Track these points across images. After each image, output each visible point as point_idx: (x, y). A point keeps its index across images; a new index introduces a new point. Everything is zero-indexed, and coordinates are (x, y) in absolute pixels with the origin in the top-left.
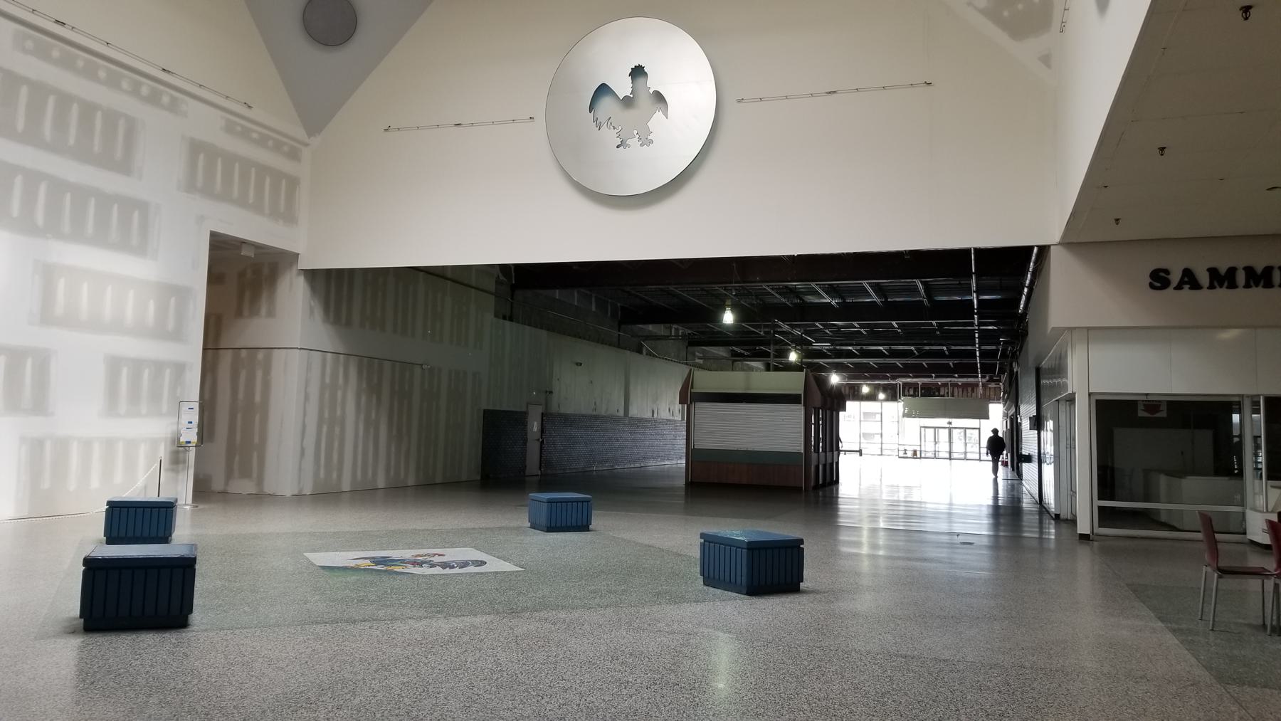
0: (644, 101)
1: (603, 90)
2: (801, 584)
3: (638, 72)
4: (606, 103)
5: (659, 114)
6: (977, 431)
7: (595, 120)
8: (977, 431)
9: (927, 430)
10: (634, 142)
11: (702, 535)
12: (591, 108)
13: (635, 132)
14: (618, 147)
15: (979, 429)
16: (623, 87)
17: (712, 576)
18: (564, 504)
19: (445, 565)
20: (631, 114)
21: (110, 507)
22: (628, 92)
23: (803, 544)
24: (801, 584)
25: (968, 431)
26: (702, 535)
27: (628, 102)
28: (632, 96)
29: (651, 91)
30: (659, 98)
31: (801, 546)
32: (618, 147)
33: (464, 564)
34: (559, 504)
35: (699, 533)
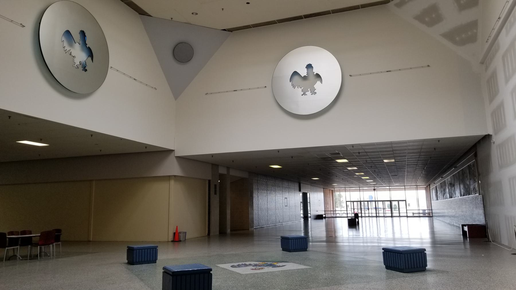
0: (312, 78)
1: (295, 73)
2: (426, 267)
3: (309, 66)
4: (296, 78)
5: (318, 83)
6: (405, 202)
7: (293, 85)
8: (405, 202)
9: (379, 202)
10: (309, 93)
11: (128, 247)
12: (291, 80)
13: (309, 89)
14: (302, 95)
15: (405, 201)
16: (303, 72)
17: (411, 267)
18: (301, 240)
19: (246, 265)
20: (306, 83)
21: (128, 249)
22: (305, 74)
23: (426, 251)
24: (426, 267)
25: (400, 202)
26: (128, 247)
27: (305, 78)
28: (307, 75)
29: (315, 74)
30: (318, 76)
31: (425, 252)
32: (302, 95)
33: (239, 266)
34: (297, 240)
35: (127, 246)
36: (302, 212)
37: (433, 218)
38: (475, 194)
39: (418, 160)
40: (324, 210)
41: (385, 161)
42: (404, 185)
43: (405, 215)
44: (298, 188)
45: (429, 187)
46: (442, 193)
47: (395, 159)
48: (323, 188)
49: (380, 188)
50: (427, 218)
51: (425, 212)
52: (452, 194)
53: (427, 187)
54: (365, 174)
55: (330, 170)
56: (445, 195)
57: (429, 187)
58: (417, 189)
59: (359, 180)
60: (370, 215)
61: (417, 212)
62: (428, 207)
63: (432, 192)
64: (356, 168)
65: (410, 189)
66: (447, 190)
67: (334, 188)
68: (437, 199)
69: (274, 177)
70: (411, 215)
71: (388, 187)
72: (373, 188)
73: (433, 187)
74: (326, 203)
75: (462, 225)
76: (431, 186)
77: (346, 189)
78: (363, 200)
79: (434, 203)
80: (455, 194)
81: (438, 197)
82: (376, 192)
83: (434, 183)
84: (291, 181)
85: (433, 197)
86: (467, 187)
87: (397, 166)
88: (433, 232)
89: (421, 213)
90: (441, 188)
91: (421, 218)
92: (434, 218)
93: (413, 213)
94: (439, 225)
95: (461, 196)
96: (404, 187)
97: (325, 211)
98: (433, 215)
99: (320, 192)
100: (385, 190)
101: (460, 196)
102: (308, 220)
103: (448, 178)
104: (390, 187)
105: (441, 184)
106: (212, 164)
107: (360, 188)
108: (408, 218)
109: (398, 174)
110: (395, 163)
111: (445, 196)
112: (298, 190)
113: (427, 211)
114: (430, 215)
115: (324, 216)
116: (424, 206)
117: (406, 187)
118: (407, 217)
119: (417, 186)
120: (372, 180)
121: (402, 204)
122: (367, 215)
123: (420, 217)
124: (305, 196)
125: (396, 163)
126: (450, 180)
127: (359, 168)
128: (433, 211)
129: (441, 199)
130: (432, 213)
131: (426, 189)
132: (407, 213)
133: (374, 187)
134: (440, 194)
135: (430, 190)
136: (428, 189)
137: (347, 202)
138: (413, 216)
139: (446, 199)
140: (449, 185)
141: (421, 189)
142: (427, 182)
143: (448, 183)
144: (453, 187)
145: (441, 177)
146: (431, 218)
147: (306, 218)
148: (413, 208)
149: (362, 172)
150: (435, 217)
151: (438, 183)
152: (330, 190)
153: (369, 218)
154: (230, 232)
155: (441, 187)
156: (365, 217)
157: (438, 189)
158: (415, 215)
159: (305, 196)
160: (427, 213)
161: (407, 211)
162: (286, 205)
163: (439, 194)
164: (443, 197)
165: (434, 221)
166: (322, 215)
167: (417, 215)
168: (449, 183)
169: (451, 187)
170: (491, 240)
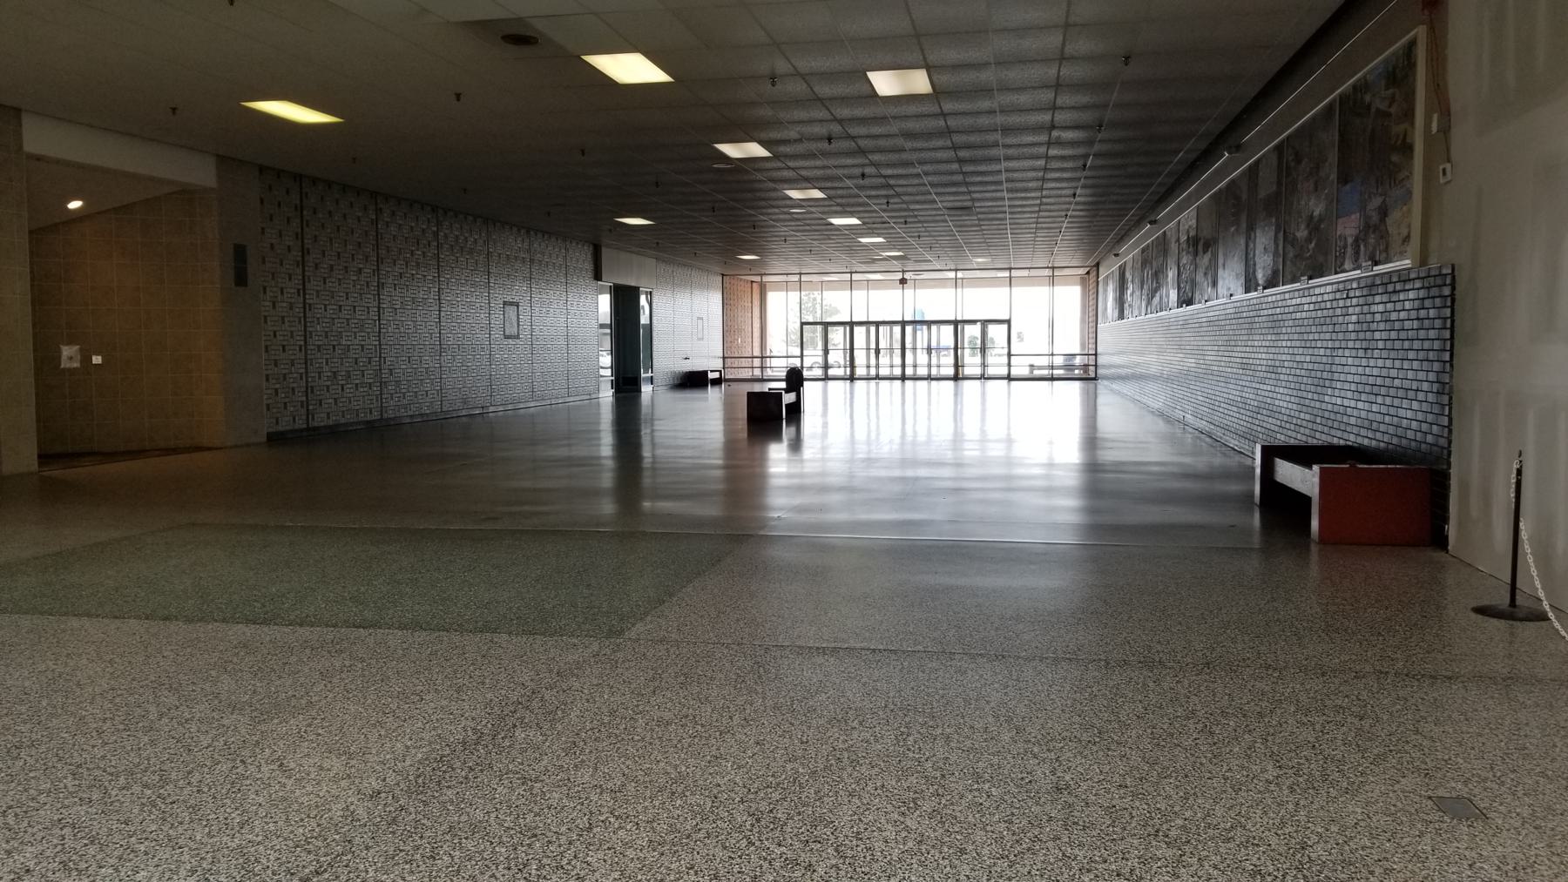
15: (1008, 322)
36: (606, 360)
37: (1099, 386)
38: (1376, 263)
39: (1058, 86)
40: (722, 355)
41: (885, 83)
42: (1006, 267)
43: (1004, 371)
44: (589, 266)
45: (1093, 274)
46: (1145, 287)
47: (930, 69)
48: (723, 275)
49: (926, 275)
50: (1077, 384)
51: (1071, 363)
52: (1194, 284)
53: (1088, 273)
54: (830, 198)
55: (774, 226)
56: (1158, 295)
57: (1095, 273)
58: (1052, 281)
59: (870, 258)
60: (934, 372)
61: (1044, 361)
62: (1083, 345)
63: (1105, 291)
64: (817, 194)
65: (1030, 281)
66: (1171, 274)
67: (761, 275)
68: (1121, 316)
69: (434, 209)
70: (1025, 372)
71: (952, 275)
72: (899, 276)
73: (1109, 269)
74: (729, 330)
75: (1264, 448)
76: (1101, 269)
77: (804, 278)
78: (865, 320)
79: (1109, 330)
80: (1215, 284)
81: (1126, 305)
82: (909, 292)
83: (1116, 255)
84: (544, 233)
85: (1106, 309)
86: (1302, 233)
87: (958, 139)
88: (1091, 440)
89: (1059, 368)
90: (1143, 271)
91: (1055, 383)
92: (1102, 384)
93: (1032, 366)
94: (1116, 416)
95: (1247, 291)
96: (1006, 274)
97: (724, 358)
98: (1100, 371)
99: (708, 287)
100: (942, 283)
101: (1241, 289)
102: (640, 391)
103: (1182, 219)
104: (960, 274)
105: (1143, 251)
106: (262, 169)
107: (855, 277)
108: (1013, 383)
109: (973, 200)
110: (935, 109)
111: (1156, 300)
112: (590, 274)
113: (1078, 361)
114: (1087, 373)
115: (711, 376)
116: (1070, 341)
117: (1014, 273)
118: (1009, 378)
119: (1053, 268)
120: (879, 235)
121: (997, 333)
122: (922, 371)
123: (1052, 379)
124: (625, 301)
125: (948, 106)
126: (1194, 221)
127: (832, 192)
128: (1101, 360)
129: (1136, 312)
130: (1096, 366)
131: (1084, 282)
132: (1009, 365)
133: (903, 271)
134: (1138, 293)
135: (1098, 282)
136: (1090, 281)
137: (803, 324)
138: (1031, 376)
139: (1159, 314)
140: (1185, 246)
141: (1067, 281)
142: (1089, 253)
143: (1178, 240)
144: (1204, 253)
145: (1151, 223)
146: (1091, 384)
147: (627, 382)
148: (1032, 345)
149: (807, 179)
150: (1106, 383)
151: (1130, 253)
152: (752, 282)
153: (877, 384)
154: (39, 467)
155: (1145, 263)
156: (915, 378)
157: (1128, 276)
158: (1037, 373)
159: (625, 301)
160: (1078, 367)
161: (799, 354)
162: (700, 336)
163: (1132, 295)
164: (1149, 303)
165: (1098, 391)
166: (705, 373)
167: (1045, 372)
168: (1184, 238)
169: (1196, 254)
170: (1547, 608)
